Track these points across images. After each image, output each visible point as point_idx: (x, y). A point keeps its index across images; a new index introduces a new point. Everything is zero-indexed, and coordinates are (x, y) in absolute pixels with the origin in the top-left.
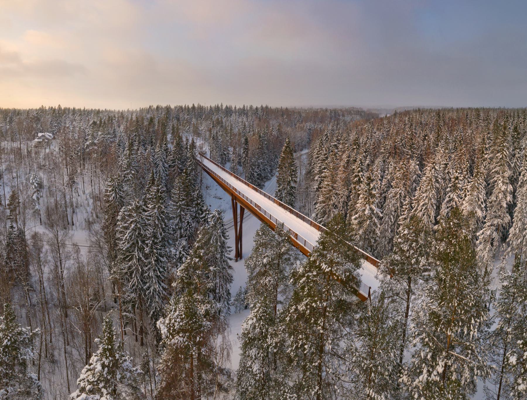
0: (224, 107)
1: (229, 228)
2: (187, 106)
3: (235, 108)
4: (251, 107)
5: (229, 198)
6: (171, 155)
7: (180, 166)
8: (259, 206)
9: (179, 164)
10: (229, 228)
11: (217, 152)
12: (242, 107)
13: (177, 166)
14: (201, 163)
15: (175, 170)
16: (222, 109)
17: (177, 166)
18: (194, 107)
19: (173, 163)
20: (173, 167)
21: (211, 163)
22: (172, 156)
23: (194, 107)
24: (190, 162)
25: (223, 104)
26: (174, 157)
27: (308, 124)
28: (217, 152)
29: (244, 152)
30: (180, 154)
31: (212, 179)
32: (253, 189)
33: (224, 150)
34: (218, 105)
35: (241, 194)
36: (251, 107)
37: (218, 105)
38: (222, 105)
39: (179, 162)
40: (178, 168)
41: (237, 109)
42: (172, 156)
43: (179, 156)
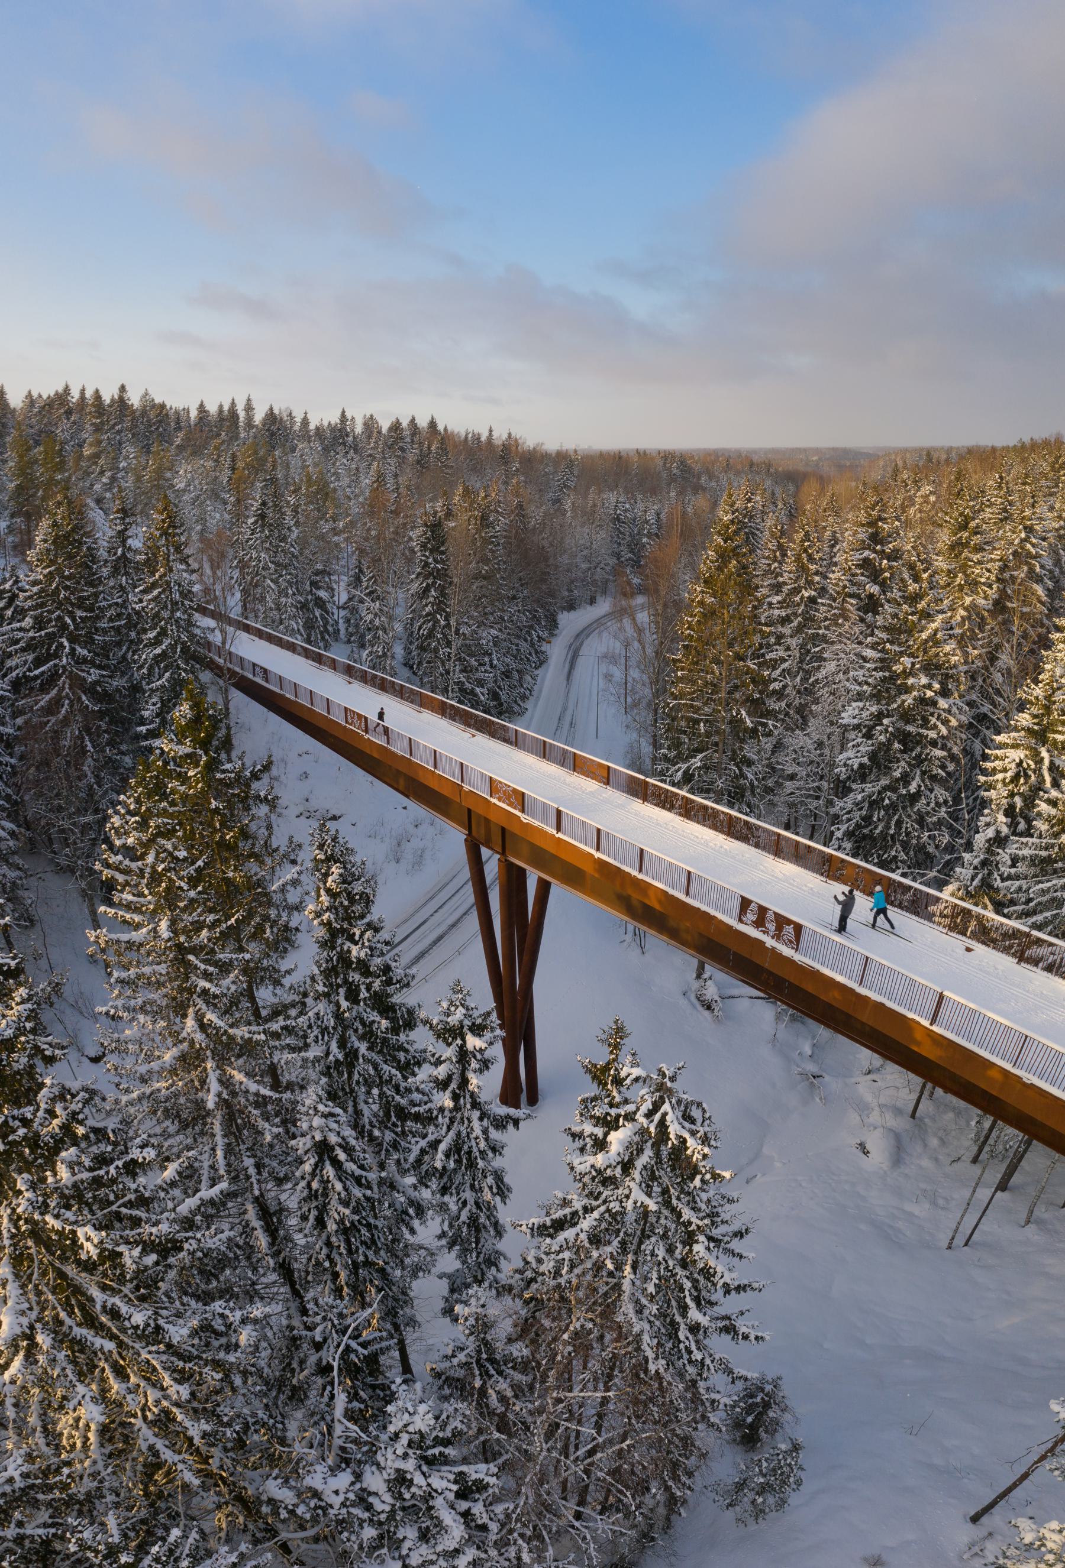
0: (259, 417)
1: (422, 955)
2: (89, 394)
3: (305, 422)
4: (370, 424)
5: (455, 837)
6: (21, 613)
7: (93, 675)
8: (360, 716)
9: (85, 661)
10: (422, 955)
11: (282, 593)
12: (335, 419)
13: (72, 676)
14: (220, 651)
15: (57, 703)
16: (249, 423)
17: (72, 676)
18: (121, 403)
19: (38, 662)
20: (44, 689)
21: (264, 643)
22: (28, 622)
23: (121, 403)
24: (157, 642)
25: (254, 404)
26: (40, 623)
27: (612, 497)
28: (282, 593)
29: (427, 589)
30: (81, 604)
31: (274, 718)
32: (443, 713)
33: (313, 584)
34: (233, 404)
35: (272, 678)
36: (370, 424)
37: (233, 404)
38: (249, 408)
39: (81, 651)
40: (77, 683)
41: (312, 427)
42: (28, 622)
43: (79, 613)
